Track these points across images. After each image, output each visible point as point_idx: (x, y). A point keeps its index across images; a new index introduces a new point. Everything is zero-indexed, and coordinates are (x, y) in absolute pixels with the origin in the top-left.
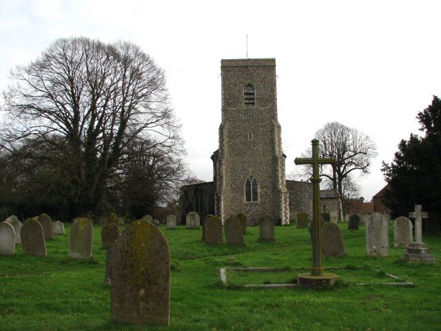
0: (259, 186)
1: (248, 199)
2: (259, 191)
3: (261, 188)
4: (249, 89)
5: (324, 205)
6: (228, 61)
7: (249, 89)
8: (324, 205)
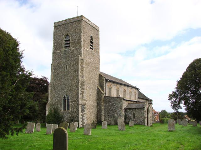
0: (70, 100)
1: (65, 109)
2: (70, 103)
3: (72, 102)
4: (71, 37)
5: (134, 114)
6: (57, 23)
7: (71, 37)
8: (134, 114)
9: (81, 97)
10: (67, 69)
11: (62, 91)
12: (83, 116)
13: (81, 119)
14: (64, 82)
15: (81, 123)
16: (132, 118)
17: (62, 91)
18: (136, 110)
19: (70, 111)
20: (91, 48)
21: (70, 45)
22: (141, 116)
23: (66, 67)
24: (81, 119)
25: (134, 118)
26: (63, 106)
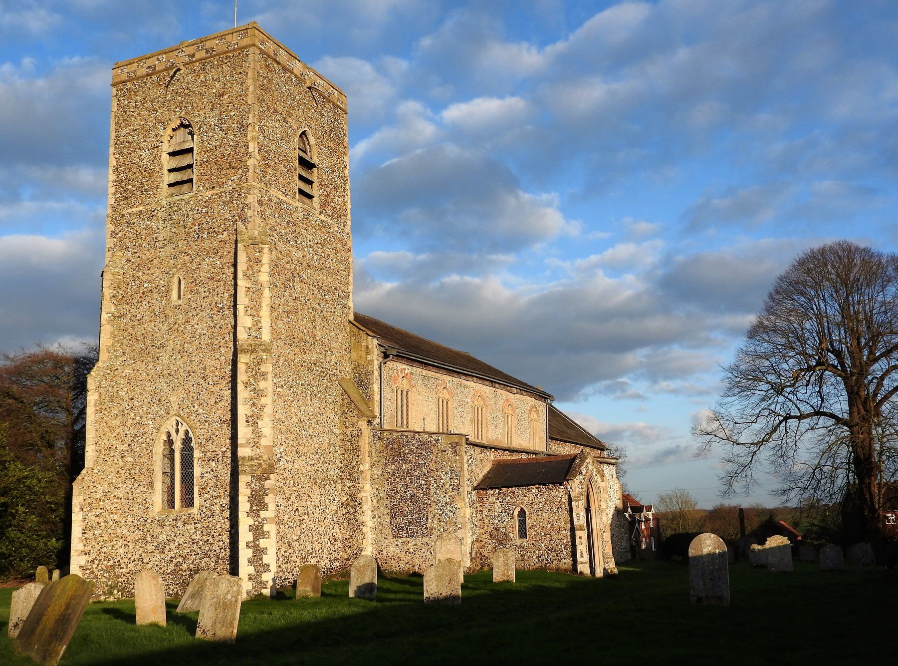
2: (197, 471)
5: (522, 513)
8: (522, 513)
9: (250, 435)
10: (179, 298)
11: (155, 408)
12: (258, 531)
13: (248, 546)
14: (166, 362)
15: (251, 570)
16: (514, 534)
17: (155, 408)
18: (531, 496)
19: (195, 511)
20: (301, 192)
21: (167, 162)
22: (556, 525)
23: (175, 287)
24: (248, 546)
25: (523, 534)
26: (159, 486)
